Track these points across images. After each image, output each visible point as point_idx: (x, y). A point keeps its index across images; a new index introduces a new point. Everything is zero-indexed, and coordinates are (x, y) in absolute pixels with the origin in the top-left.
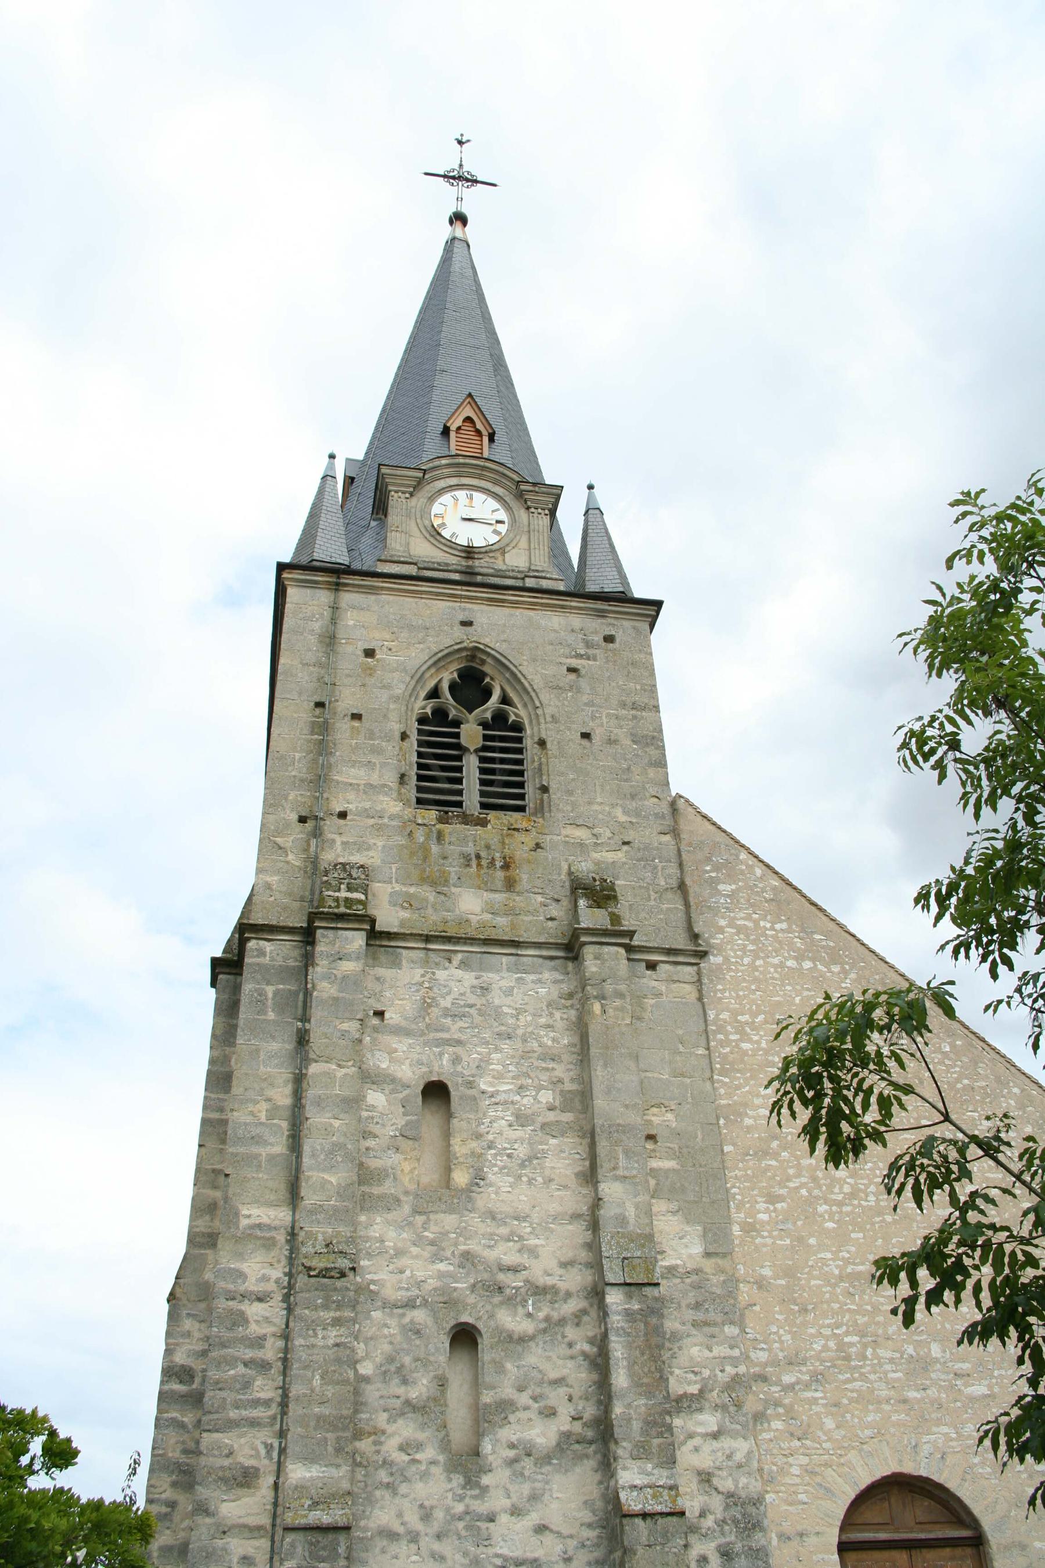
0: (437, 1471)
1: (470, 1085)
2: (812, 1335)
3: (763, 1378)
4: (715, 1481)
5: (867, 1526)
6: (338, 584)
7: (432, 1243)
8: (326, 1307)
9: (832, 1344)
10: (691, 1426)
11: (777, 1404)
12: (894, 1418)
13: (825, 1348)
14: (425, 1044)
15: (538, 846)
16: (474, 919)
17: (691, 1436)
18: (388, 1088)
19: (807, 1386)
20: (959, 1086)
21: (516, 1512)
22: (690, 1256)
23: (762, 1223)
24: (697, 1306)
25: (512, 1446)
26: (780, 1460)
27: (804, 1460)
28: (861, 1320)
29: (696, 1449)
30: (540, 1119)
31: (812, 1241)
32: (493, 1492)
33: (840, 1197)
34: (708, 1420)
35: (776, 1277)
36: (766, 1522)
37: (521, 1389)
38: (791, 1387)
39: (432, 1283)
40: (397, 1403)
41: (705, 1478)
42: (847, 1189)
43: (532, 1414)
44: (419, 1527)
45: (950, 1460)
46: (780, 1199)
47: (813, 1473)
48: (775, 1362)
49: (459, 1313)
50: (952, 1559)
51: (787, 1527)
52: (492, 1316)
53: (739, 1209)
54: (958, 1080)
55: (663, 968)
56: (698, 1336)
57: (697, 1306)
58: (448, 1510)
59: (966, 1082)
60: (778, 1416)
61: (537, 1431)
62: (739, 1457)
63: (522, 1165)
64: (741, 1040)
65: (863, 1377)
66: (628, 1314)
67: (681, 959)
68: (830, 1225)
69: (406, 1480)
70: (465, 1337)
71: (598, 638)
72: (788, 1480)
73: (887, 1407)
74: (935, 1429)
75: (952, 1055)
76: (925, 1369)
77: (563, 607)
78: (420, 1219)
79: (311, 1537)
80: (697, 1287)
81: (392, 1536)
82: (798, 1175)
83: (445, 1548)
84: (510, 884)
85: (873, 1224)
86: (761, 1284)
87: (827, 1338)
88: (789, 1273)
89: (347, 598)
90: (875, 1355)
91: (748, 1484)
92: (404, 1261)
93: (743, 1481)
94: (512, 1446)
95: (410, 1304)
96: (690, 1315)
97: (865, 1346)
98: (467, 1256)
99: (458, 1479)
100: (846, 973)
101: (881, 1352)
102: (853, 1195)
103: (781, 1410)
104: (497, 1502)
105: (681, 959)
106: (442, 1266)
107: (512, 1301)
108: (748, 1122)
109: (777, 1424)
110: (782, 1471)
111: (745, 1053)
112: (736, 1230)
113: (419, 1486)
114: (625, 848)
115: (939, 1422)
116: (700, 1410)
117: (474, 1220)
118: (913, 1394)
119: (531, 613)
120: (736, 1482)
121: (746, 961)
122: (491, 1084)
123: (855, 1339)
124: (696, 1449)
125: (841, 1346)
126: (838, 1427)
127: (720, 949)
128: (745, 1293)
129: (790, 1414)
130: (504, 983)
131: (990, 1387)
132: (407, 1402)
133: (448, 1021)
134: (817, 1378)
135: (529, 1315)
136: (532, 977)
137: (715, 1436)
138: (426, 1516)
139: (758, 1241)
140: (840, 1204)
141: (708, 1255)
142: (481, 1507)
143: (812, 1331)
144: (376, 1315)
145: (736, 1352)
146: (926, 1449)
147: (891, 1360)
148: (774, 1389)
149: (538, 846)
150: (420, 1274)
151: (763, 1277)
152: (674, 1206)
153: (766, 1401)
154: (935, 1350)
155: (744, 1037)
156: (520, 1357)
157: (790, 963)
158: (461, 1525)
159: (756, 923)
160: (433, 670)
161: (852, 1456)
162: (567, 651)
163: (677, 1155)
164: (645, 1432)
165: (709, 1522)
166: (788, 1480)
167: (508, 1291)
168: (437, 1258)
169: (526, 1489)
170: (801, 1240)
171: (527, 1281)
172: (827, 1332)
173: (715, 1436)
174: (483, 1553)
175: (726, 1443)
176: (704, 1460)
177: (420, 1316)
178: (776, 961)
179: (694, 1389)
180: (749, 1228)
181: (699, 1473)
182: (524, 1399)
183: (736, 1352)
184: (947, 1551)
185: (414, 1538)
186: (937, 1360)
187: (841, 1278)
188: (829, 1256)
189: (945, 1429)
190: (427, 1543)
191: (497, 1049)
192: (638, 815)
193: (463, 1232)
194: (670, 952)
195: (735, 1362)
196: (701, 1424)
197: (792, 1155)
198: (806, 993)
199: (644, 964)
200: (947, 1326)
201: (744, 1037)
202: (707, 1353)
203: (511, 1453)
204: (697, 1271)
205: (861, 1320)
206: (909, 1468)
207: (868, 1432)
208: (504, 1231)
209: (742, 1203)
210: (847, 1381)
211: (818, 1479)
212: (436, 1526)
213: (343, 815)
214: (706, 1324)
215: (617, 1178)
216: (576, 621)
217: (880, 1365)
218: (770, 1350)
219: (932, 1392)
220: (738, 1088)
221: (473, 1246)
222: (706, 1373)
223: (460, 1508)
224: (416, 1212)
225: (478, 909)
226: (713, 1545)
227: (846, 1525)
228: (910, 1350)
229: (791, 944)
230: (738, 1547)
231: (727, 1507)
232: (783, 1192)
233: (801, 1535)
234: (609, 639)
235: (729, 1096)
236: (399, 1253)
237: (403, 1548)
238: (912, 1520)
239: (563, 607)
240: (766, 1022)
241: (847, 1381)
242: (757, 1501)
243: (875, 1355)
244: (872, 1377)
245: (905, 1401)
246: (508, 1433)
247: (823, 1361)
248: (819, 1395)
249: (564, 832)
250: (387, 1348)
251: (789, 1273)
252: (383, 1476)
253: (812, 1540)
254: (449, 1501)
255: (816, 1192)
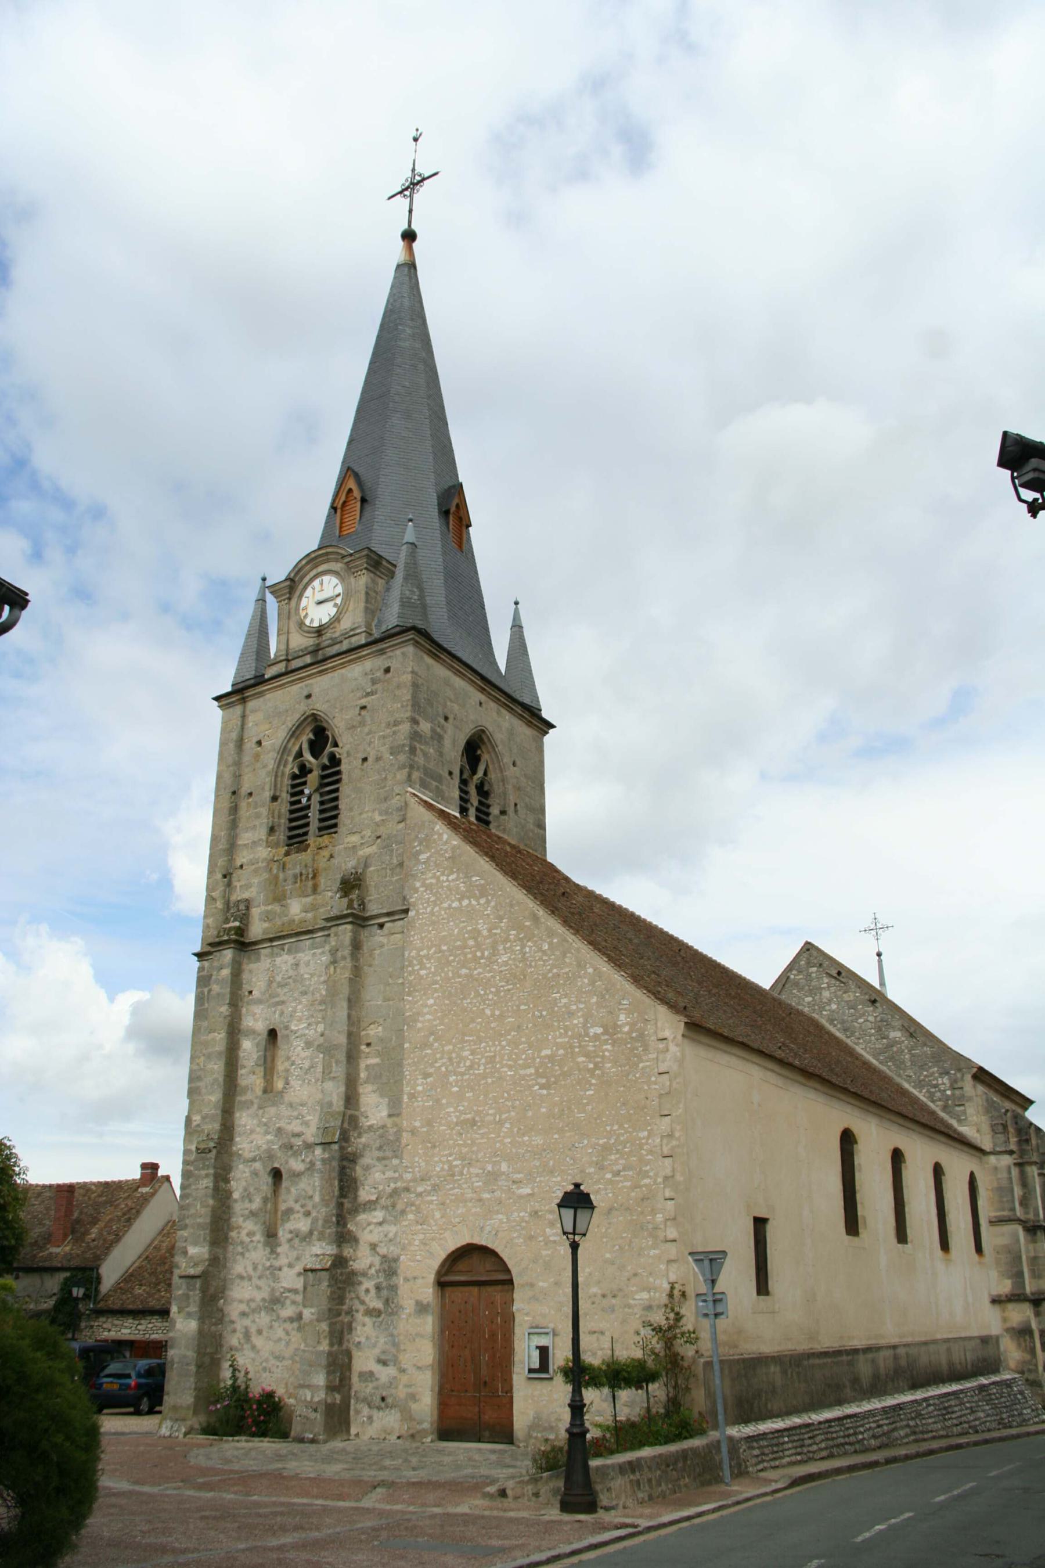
0: (260, 1245)
1: (287, 1028)
2: (436, 1162)
3: (407, 1189)
4: (378, 1249)
5: (461, 1272)
6: (243, 698)
7: (265, 1124)
8: (203, 1169)
9: (446, 1167)
10: (371, 1219)
11: (412, 1205)
12: (474, 1210)
13: (442, 1169)
14: (269, 1007)
15: (331, 856)
16: (296, 918)
17: (369, 1224)
18: (251, 1037)
19: (429, 1193)
20: (550, 975)
21: (290, 1266)
22: (381, 1118)
23: (419, 1092)
24: (380, 1148)
25: (291, 1232)
26: (410, 1237)
27: (421, 1236)
28: (464, 1150)
29: (371, 1232)
30: (316, 1043)
31: (444, 1101)
32: (281, 1256)
33: (463, 1070)
34: (378, 1215)
35: (422, 1126)
36: (399, 1271)
37: (296, 1202)
38: (420, 1195)
39: (265, 1147)
40: (247, 1212)
41: (373, 1247)
42: (468, 1063)
43: (300, 1215)
44: (252, 1273)
45: (500, 1235)
46: (429, 1075)
47: (425, 1244)
48: (414, 1180)
49: (273, 1162)
50: (501, 1291)
51: (409, 1275)
52: (287, 1163)
53: (407, 1084)
54: (550, 971)
55: (387, 925)
56: (379, 1166)
57: (380, 1148)
58: (263, 1265)
59: (555, 971)
60: (412, 1212)
61: (302, 1224)
62: (391, 1235)
63: (306, 1073)
64: (421, 969)
65: (460, 1187)
66: (323, 1160)
67: (397, 917)
68: (455, 1089)
69: (248, 1250)
70: (277, 1175)
71: (379, 674)
72: (412, 1248)
73: (470, 1204)
74: (495, 1217)
75: (549, 952)
76: (496, 1180)
77: (360, 658)
78: (261, 1111)
79: (188, 1280)
80: (381, 1136)
81: (242, 1277)
82: (442, 1058)
83: (260, 1283)
84: (315, 889)
85: (479, 1085)
86: (413, 1132)
87: (444, 1163)
88: (429, 1123)
89: (251, 704)
90: (469, 1172)
91: (393, 1250)
92: (254, 1136)
93: (392, 1248)
94: (291, 1232)
95: (254, 1160)
96: (377, 1154)
97: (463, 1167)
98: (279, 1130)
99: (268, 1250)
100: (488, 902)
101: (472, 1170)
102: (471, 1067)
103: (413, 1208)
104: (283, 1261)
105: (397, 917)
106: (269, 1137)
107: (296, 1154)
108: (419, 1025)
109: (411, 1216)
110: (410, 1244)
111: (421, 977)
112: (405, 1098)
113: (253, 1253)
114: (379, 841)
115: (498, 1212)
116: (375, 1209)
117: (283, 1108)
118: (486, 1196)
119: (343, 671)
120: (388, 1249)
121: (429, 909)
122: (296, 1025)
123: (459, 1162)
124: (371, 1232)
125: (451, 1167)
126: (442, 1217)
127: (415, 904)
128: (406, 1137)
129: (418, 1211)
130: (306, 958)
131: (533, 1189)
132: (251, 1212)
133: (279, 990)
134: (435, 1188)
135: (303, 1161)
136: (320, 951)
137: (380, 1224)
138: (255, 1268)
139: (416, 1104)
140: (463, 1074)
141: (390, 1116)
142: (277, 1264)
143: (436, 1159)
144: (241, 1166)
145: (397, 1175)
146: (488, 1228)
147: (477, 1175)
148: (413, 1195)
149: (331, 856)
150: (260, 1142)
151: (415, 1128)
152: (375, 1088)
153: (407, 1203)
154: (504, 1167)
155: (423, 966)
156: (297, 1184)
157: (455, 904)
158: (268, 1272)
159: (438, 879)
160: (293, 740)
161: (447, 1234)
162: (359, 694)
163: (379, 1054)
164: (323, 1226)
165: (373, 1271)
166: (412, 1248)
167: (295, 1148)
168: (267, 1133)
169: (295, 1253)
170: (438, 1101)
171: (304, 1142)
172: (444, 1159)
173: (380, 1224)
174: (276, 1285)
175: (386, 1228)
176: (374, 1238)
177: (258, 1165)
178: (445, 905)
179: (374, 1198)
180: (412, 1096)
181: (371, 1245)
182: (297, 1207)
183: (397, 1175)
184: (499, 1287)
185: (250, 1278)
186: (503, 1173)
187: (457, 1124)
188: (452, 1110)
189: (500, 1216)
190: (255, 1281)
191: (300, 1003)
192: (386, 813)
193: (279, 1117)
194: (388, 914)
195: (395, 1180)
196: (375, 1217)
197: (440, 1044)
198: (462, 925)
199: (376, 926)
200: (514, 1150)
201: (423, 966)
202: (382, 1176)
203: (289, 1236)
204: (384, 1127)
205: (464, 1150)
206: (477, 1240)
207: (457, 1220)
208: (295, 1113)
209: (410, 1080)
210: (452, 1189)
211: (427, 1248)
212: (259, 1273)
213: (241, 867)
214: (384, 1159)
215: (330, 1079)
216: (368, 664)
217: (470, 1178)
218: (413, 1172)
219: (498, 1194)
220: (416, 1002)
221: (282, 1124)
222: (381, 1187)
223: (268, 1264)
224: (260, 1108)
225: (298, 911)
226: (373, 1283)
227: (440, 1274)
228: (489, 1168)
229: (458, 888)
230: (384, 1284)
231: (382, 1263)
232: (432, 1070)
233: (415, 1278)
234: (387, 670)
235: (411, 1009)
236: (252, 1131)
237: (246, 1283)
238: (481, 1270)
239: (360, 658)
240: (435, 953)
241: (452, 1189)
242: (396, 1260)
243: (469, 1172)
244: (464, 1186)
245: (480, 1200)
246: (290, 1225)
247: (439, 1177)
248: (434, 1198)
249: (346, 840)
250: (244, 1183)
251: (429, 1123)
252: (240, 1249)
253: (420, 1281)
254: (264, 1261)
255: (450, 1068)
